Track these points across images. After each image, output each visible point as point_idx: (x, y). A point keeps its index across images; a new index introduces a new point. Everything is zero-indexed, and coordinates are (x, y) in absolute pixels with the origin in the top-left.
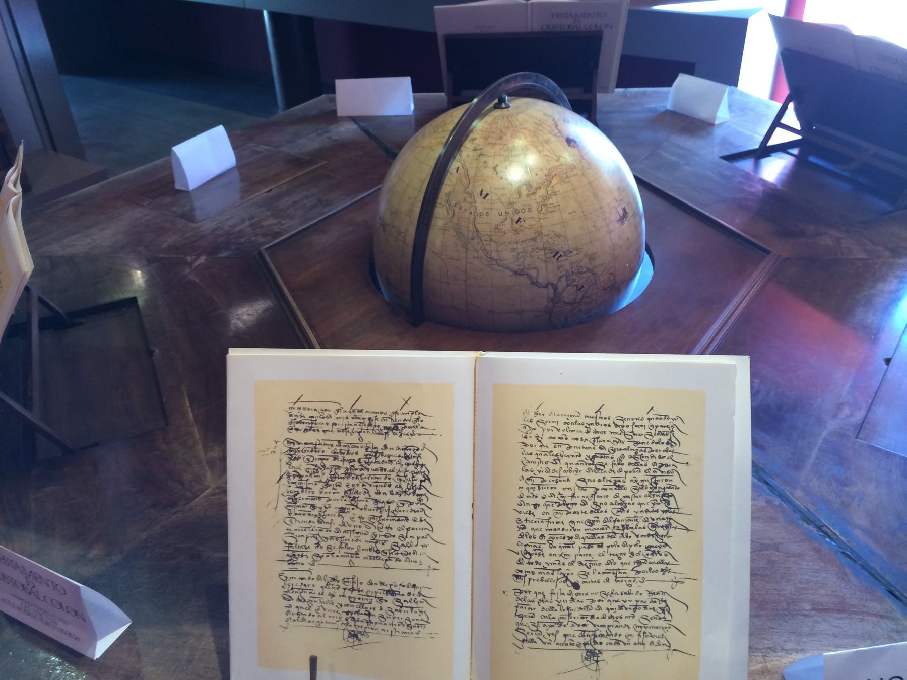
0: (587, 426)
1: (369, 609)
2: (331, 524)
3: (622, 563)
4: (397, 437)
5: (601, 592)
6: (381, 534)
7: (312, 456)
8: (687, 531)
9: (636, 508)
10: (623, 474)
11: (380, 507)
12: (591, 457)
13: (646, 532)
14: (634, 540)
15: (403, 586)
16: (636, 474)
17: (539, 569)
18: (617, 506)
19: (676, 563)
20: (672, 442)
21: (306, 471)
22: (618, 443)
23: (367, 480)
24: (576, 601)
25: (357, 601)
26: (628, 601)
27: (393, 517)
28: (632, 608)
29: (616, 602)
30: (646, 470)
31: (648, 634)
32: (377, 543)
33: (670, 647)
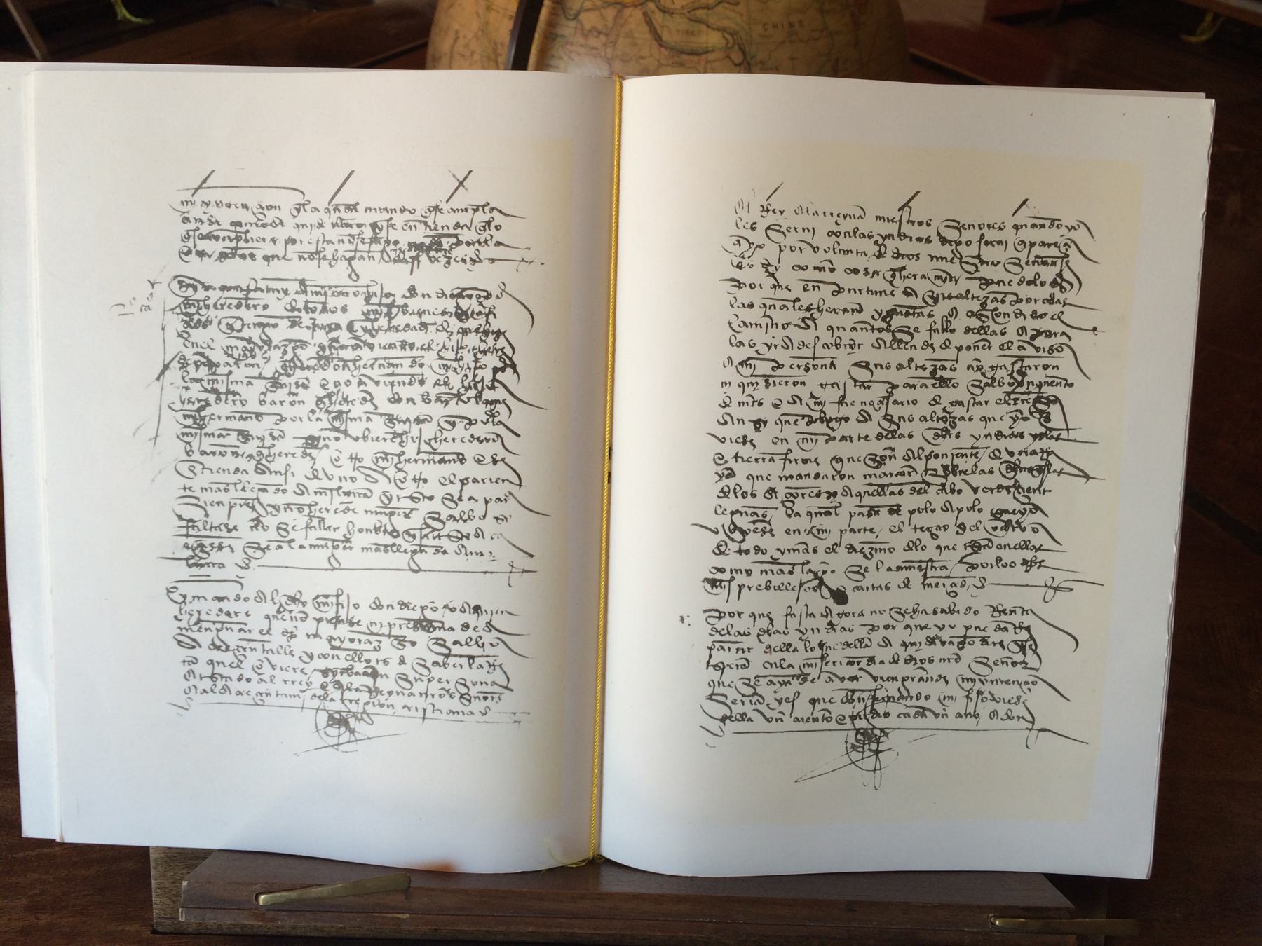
0: (881, 241)
1: (373, 663)
2: (286, 474)
3: (939, 547)
4: (439, 266)
5: (891, 610)
6: (402, 493)
7: (238, 318)
8: (1085, 480)
9: (977, 427)
10: (951, 354)
11: (401, 432)
12: (884, 313)
13: (996, 480)
14: (966, 498)
15: (453, 610)
16: (980, 354)
17: (762, 562)
18: (934, 425)
19: (1054, 546)
20: (1063, 280)
21: (226, 353)
22: (944, 281)
23: (368, 372)
24: (837, 628)
25: (347, 645)
26: (947, 628)
27: (430, 453)
28: (956, 641)
29: (922, 628)
30: (1002, 345)
31: (986, 694)
32: (392, 514)
33: (1033, 723)
